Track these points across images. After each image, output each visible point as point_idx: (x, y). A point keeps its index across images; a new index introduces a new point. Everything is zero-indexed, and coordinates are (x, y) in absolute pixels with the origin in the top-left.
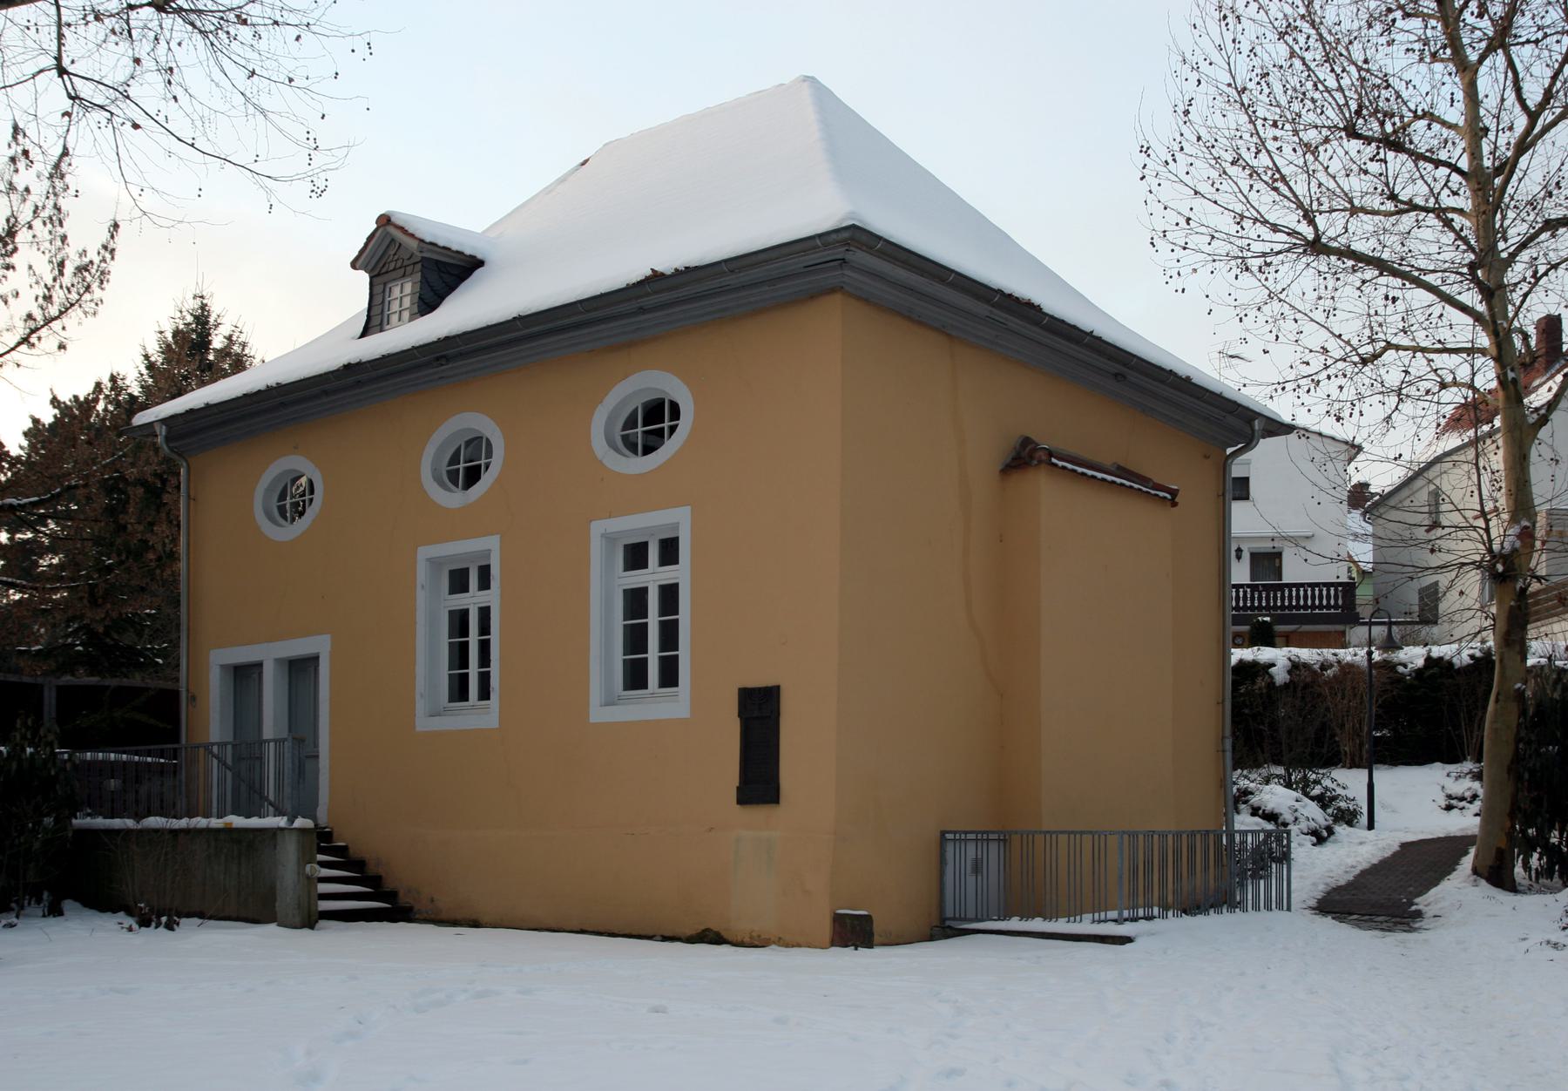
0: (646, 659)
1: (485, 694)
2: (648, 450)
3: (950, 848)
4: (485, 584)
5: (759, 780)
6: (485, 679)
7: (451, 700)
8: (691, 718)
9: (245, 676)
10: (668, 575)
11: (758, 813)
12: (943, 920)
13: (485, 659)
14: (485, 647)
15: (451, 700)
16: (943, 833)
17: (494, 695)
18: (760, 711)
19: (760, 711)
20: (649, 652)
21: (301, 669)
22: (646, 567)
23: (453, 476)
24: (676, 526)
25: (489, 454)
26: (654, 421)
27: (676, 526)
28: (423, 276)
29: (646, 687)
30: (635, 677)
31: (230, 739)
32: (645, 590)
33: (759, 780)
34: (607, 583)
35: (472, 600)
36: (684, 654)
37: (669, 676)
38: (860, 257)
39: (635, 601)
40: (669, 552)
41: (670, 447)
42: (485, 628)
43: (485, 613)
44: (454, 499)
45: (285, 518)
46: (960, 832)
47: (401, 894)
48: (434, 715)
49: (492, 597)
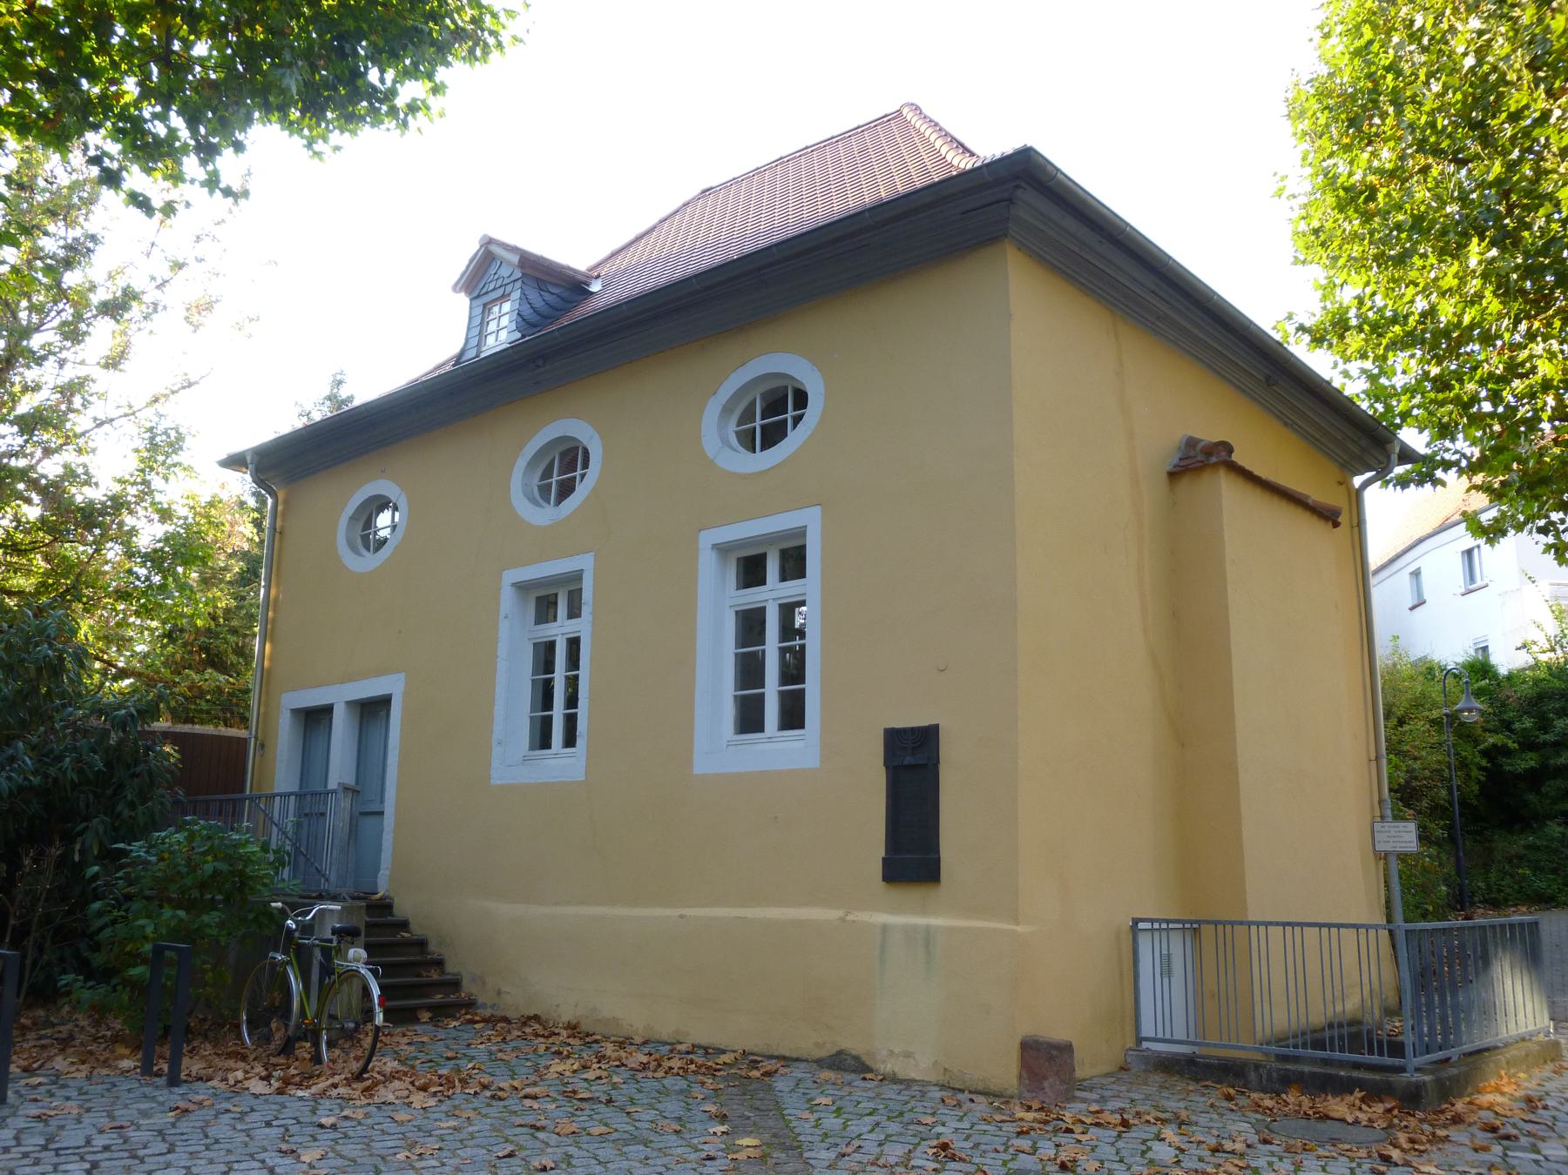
0: (803, 691)
1: (570, 741)
2: (768, 443)
3: (1145, 943)
4: (574, 612)
5: (912, 855)
6: (571, 722)
7: (532, 748)
8: (824, 765)
9: (315, 719)
10: (791, 589)
11: (912, 894)
12: (1140, 1040)
13: (572, 701)
14: (573, 683)
15: (532, 748)
16: (1136, 921)
17: (581, 742)
18: (912, 760)
19: (912, 760)
20: (771, 687)
21: (372, 710)
22: (763, 582)
23: (545, 491)
24: (801, 532)
25: (586, 465)
26: (773, 414)
27: (801, 532)
28: (523, 293)
29: (761, 730)
30: (749, 719)
31: (295, 789)
32: (761, 612)
33: (912, 855)
34: (717, 601)
35: (559, 630)
36: (812, 687)
37: (793, 716)
38: (1027, 196)
39: (751, 625)
40: (794, 563)
41: (795, 439)
42: (573, 661)
43: (574, 644)
44: (543, 516)
45: (368, 549)
46: (1160, 921)
47: (465, 983)
48: (510, 757)
49: (582, 627)
